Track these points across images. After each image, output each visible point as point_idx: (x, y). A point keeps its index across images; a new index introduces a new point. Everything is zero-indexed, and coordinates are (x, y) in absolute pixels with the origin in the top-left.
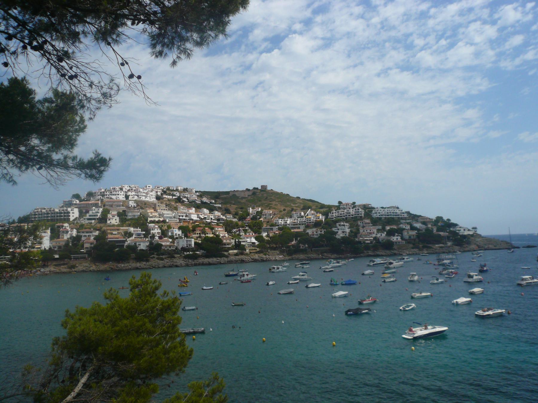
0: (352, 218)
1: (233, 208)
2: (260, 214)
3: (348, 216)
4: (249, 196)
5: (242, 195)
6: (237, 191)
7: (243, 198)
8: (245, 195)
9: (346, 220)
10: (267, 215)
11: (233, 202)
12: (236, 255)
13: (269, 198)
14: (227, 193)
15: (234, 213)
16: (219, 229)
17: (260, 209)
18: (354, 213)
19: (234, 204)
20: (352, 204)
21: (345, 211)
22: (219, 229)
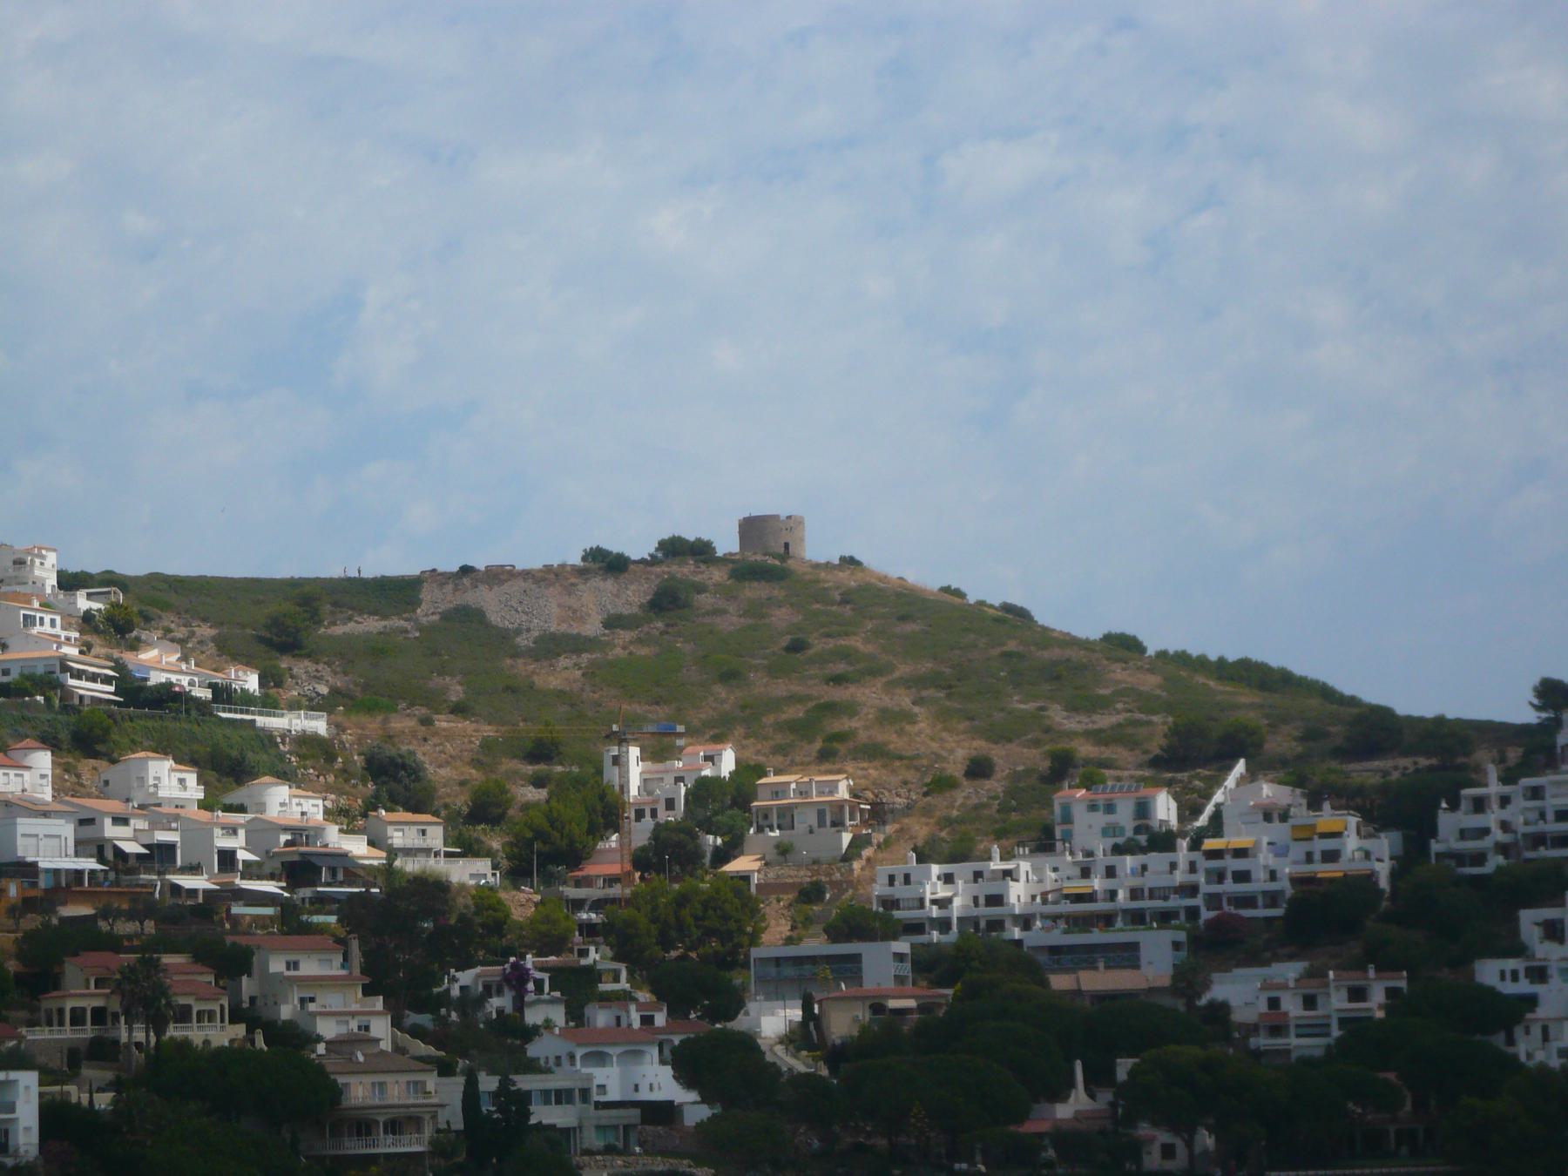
2: (722, 806)
4: (613, 622)
5: (549, 614)
6: (497, 576)
7: (552, 646)
8: (578, 615)
11: (456, 692)
13: (818, 645)
14: (395, 593)
15: (462, 802)
17: (728, 763)
19: (459, 710)
22: (310, 967)
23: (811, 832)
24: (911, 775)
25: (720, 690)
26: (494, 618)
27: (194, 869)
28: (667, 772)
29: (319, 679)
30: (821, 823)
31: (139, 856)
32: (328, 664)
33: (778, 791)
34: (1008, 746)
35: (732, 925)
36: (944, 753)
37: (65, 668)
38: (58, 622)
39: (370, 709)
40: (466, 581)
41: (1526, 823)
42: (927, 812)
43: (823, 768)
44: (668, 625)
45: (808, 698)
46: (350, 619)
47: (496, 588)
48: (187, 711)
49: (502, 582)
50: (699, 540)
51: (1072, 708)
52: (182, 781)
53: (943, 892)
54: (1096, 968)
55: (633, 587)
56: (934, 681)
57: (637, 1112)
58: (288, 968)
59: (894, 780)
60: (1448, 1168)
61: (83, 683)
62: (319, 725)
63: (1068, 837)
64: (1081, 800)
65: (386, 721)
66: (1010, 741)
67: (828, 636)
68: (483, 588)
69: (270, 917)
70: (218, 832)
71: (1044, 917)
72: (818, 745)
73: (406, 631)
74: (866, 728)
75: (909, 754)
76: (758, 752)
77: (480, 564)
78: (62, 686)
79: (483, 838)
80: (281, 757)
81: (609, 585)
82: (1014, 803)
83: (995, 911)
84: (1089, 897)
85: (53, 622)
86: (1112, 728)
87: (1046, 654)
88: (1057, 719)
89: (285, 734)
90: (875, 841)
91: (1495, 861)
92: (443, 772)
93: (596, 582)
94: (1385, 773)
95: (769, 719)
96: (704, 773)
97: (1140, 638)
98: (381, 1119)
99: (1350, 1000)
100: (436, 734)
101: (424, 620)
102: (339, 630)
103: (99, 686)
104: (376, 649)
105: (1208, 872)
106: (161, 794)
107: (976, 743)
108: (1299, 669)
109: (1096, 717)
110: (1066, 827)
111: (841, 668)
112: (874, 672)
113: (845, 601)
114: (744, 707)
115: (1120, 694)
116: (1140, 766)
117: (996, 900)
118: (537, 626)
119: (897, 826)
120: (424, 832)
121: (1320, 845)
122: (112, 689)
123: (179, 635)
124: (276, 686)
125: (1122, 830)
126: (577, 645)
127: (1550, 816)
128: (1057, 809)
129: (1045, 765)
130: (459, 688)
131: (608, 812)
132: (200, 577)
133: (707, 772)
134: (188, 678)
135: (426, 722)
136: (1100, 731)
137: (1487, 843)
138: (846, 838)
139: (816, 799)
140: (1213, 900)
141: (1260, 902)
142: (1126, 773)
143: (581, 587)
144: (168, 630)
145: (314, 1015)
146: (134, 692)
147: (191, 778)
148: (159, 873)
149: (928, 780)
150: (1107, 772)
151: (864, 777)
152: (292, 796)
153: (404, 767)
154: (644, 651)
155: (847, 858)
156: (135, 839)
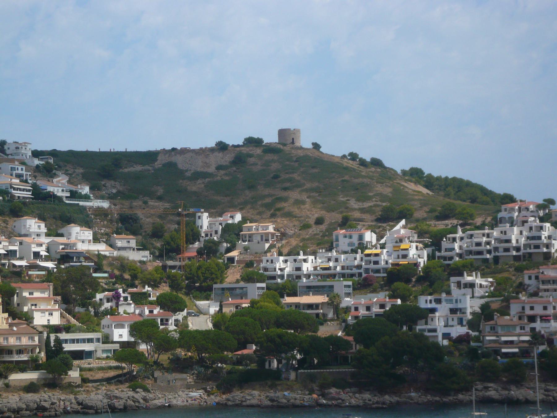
0: (516, 258)
1: (148, 212)
2: (232, 233)
3: (501, 253)
4: (219, 168)
5: (198, 165)
6: (184, 151)
7: (197, 176)
8: (207, 165)
9: (485, 267)
10: (257, 238)
11: (160, 191)
12: (31, 388)
13: (283, 176)
14: (150, 157)
15: (149, 229)
16: (37, 294)
17: (238, 217)
18: (523, 241)
19: (160, 198)
20: (540, 207)
21: (496, 233)
22: (37, 294)
24: (297, 223)
25: (247, 192)
26: (180, 166)
27: (21, 258)
28: (217, 221)
29: (114, 187)
30: (262, 239)
31: (4, 254)
33: (250, 229)
34: (333, 213)
35: (214, 276)
36: (310, 216)
37: (11, 187)
38: (24, 169)
40: (173, 153)
41: (467, 247)
42: (298, 236)
43: (271, 220)
44: (237, 169)
45: (274, 195)
46: (132, 166)
47: (182, 156)
48: (54, 201)
49: (184, 154)
50: (258, 138)
51: (358, 200)
52: (39, 226)
53: (283, 266)
54: (309, 295)
55: (228, 155)
56: (317, 190)
57: (118, 345)
58: (30, 295)
59: (291, 225)
60: (353, 370)
61: (19, 192)
62: (105, 204)
63: (337, 246)
64: (342, 234)
65: (131, 202)
66: (333, 212)
67: (287, 173)
68: (178, 156)
69: (43, 275)
70: (33, 246)
71: (314, 275)
72: (272, 211)
73: (150, 170)
75: (298, 215)
76: (252, 214)
78: (11, 193)
79: (154, 243)
80: (88, 216)
81: (221, 155)
82: (327, 233)
83: (298, 273)
84: (329, 269)
85: (22, 169)
87: (356, 181)
88: (352, 204)
89: (91, 208)
90: (277, 246)
92: (148, 220)
93: (216, 154)
94: (447, 225)
95: (260, 203)
96: (228, 222)
97: (423, 169)
98: (14, 350)
99: (380, 308)
100: (148, 207)
102: (126, 170)
103: (25, 193)
105: (366, 261)
106: (31, 230)
107: (322, 212)
108: (474, 181)
109: (364, 203)
110: (337, 243)
111: (288, 185)
112: (297, 186)
113: (296, 161)
114: (252, 198)
115: (377, 195)
116: (372, 221)
117: (299, 269)
119: (287, 241)
120: (129, 242)
121: (401, 253)
122: (31, 193)
123: (70, 172)
124: (98, 190)
125: (354, 244)
126: (204, 175)
127: (474, 245)
128: (334, 237)
129: (340, 220)
130: (162, 190)
133: (230, 222)
134: (61, 189)
135: (145, 203)
138: (267, 245)
139: (260, 232)
140: (367, 270)
141: (382, 271)
142: (367, 223)
143: (211, 155)
144: (67, 170)
145: (33, 310)
146: (40, 196)
147: (43, 225)
148: (9, 260)
149: (302, 225)
150: (361, 223)
151: (282, 224)
152: (81, 230)
153: (131, 218)
154: (227, 178)
155: (266, 252)
156: (3, 249)
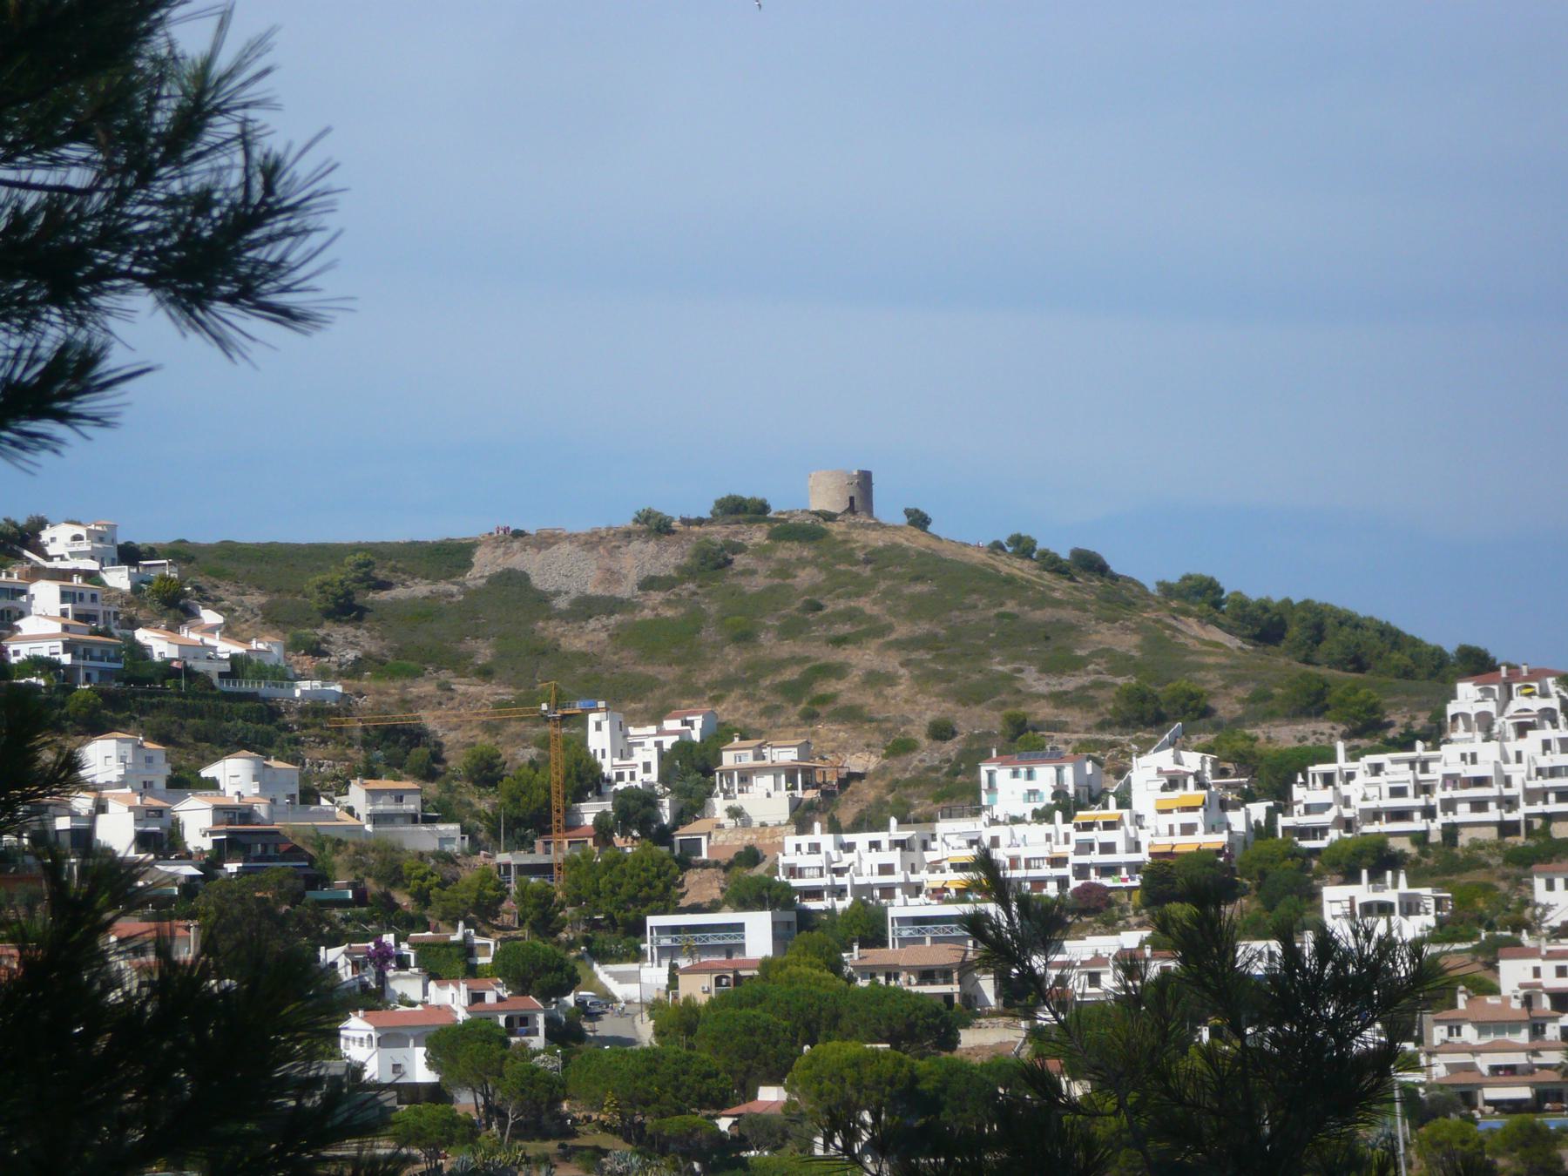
4: (648, 584)
7: (586, 608)
8: (612, 576)
11: (484, 652)
13: (833, 605)
14: (451, 557)
19: (486, 673)
23: (769, 795)
25: (730, 652)
26: (536, 581)
32: (369, 630)
36: (912, 717)
39: (393, 674)
40: (516, 545)
45: (807, 659)
51: (1047, 669)
55: (673, 549)
73: (452, 596)
74: (849, 689)
75: (880, 717)
77: (531, 528)
81: (652, 547)
86: (1077, 689)
91: (1334, 834)
92: (452, 735)
101: (470, 584)
104: (425, 612)
107: (945, 706)
109: (1064, 679)
111: (843, 629)
113: (867, 562)
118: (574, 588)
126: (611, 605)
131: (588, 780)
132: (271, 544)
136: (1066, 693)
137: (1327, 817)
140: (1082, 871)
142: (1075, 736)
